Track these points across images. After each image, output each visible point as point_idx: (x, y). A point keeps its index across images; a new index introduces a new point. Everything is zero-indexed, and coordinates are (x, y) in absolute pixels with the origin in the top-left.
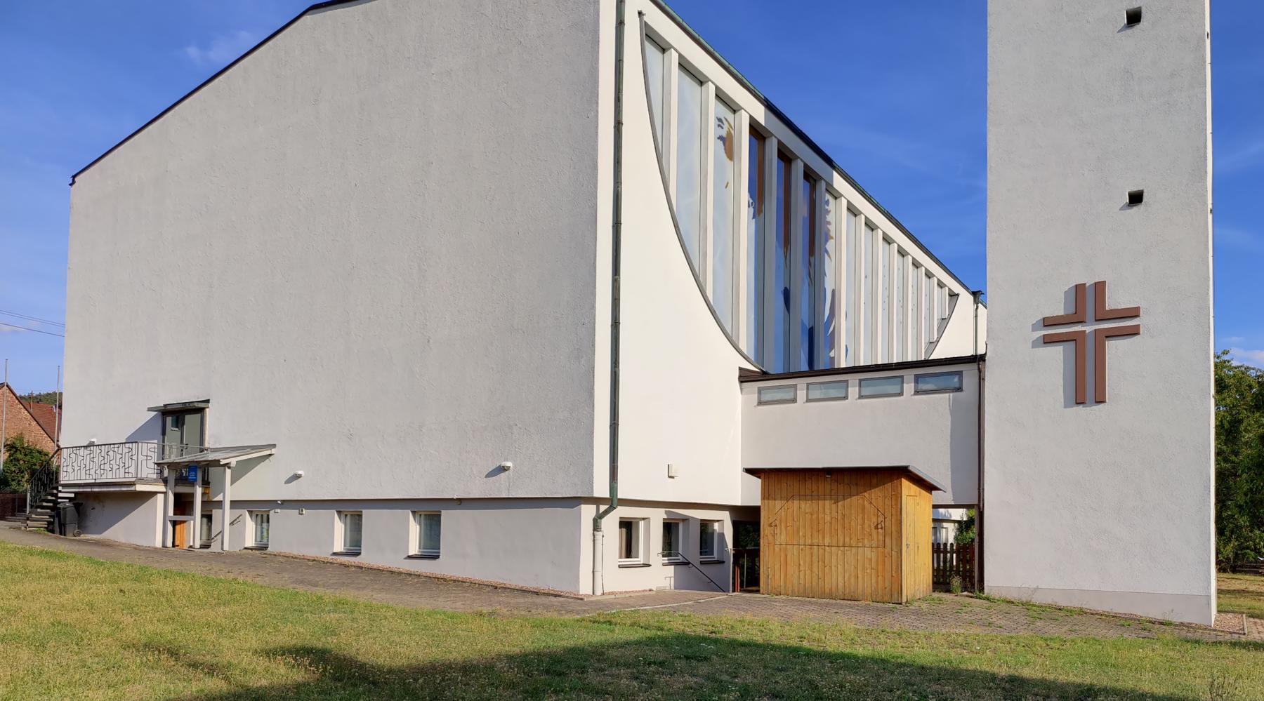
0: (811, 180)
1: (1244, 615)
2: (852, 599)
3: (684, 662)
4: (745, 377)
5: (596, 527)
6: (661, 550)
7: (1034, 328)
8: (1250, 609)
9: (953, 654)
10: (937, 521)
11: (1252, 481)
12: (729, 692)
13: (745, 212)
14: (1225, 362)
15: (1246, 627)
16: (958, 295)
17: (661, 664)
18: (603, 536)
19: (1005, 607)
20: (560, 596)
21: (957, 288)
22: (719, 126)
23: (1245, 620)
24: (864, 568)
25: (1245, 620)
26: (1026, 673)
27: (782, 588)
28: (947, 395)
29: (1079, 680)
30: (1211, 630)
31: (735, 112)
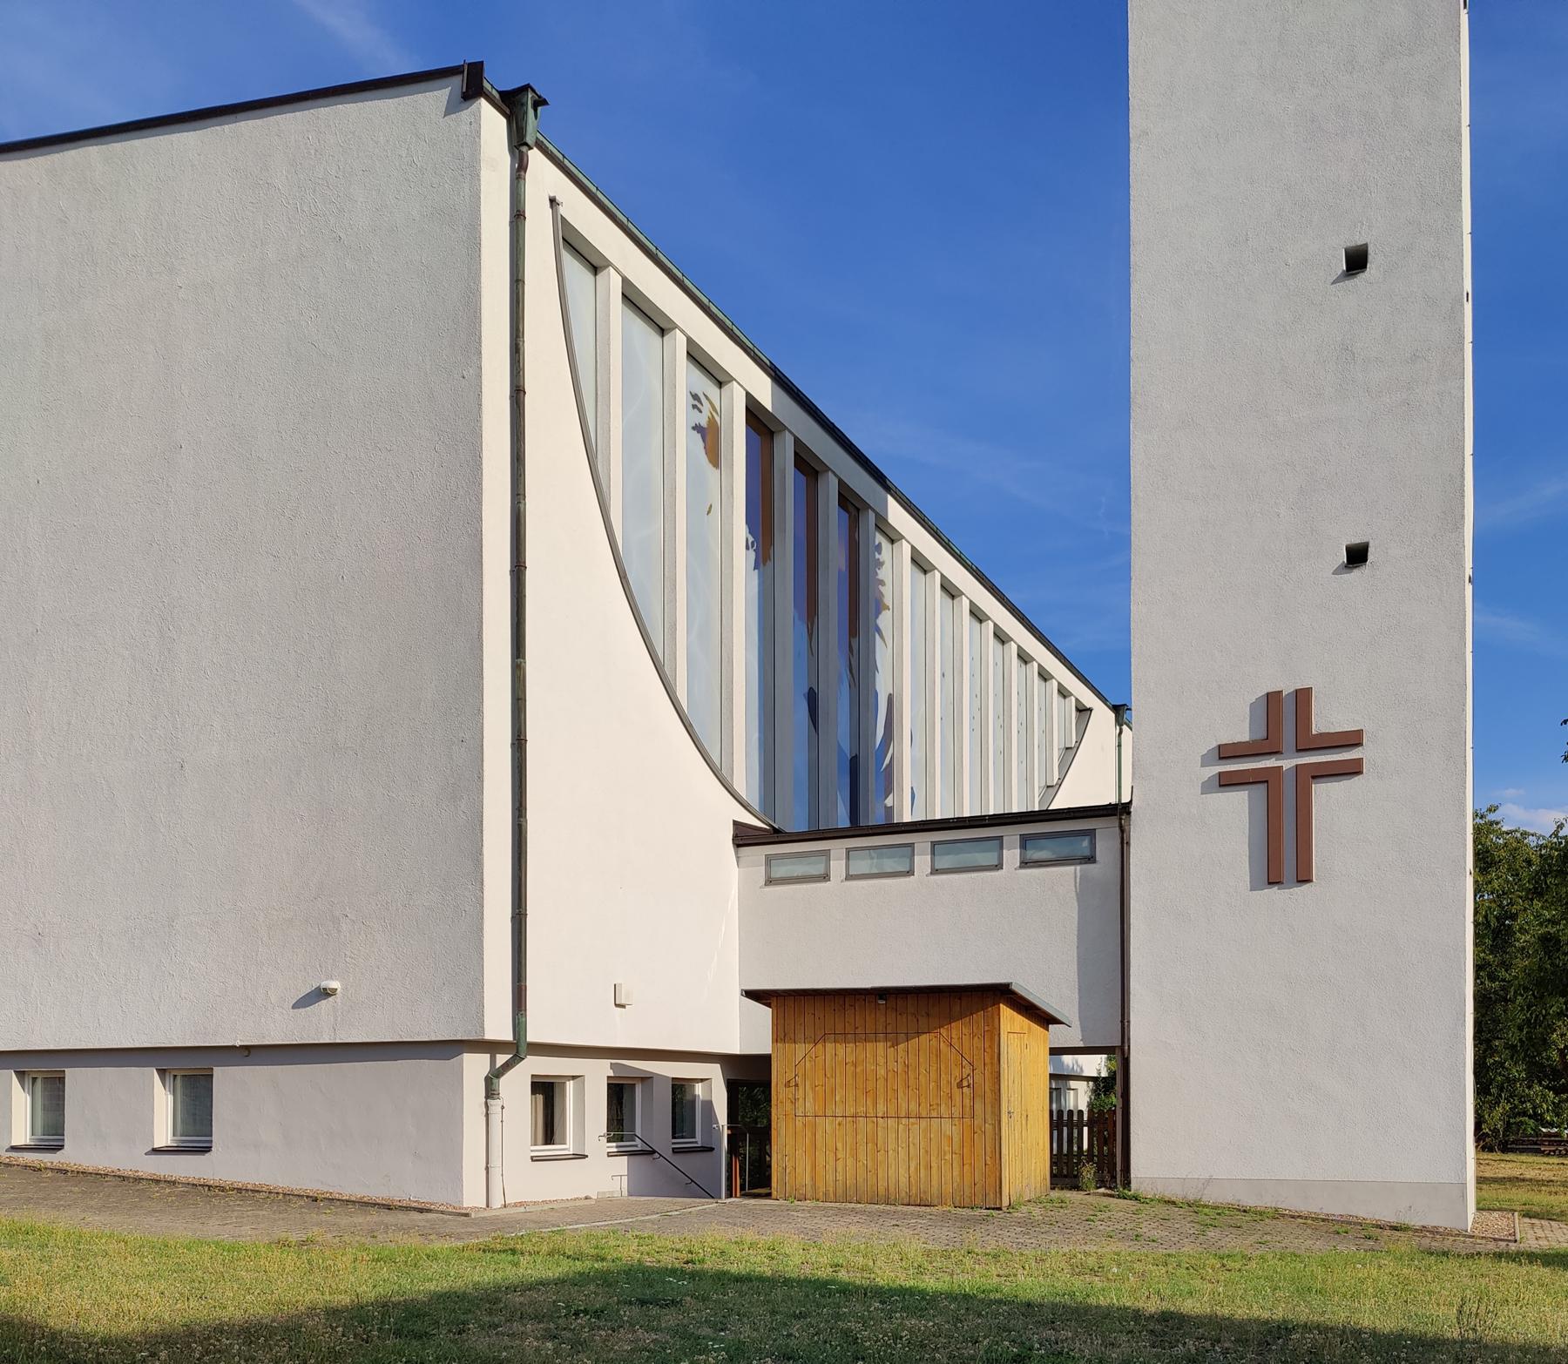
0: (851, 509)
1: (1516, 1214)
2: (923, 1203)
3: (636, 1309)
4: (744, 837)
5: (491, 1092)
6: (604, 1130)
7: (1205, 762)
8: (1525, 1204)
9: (1078, 1283)
10: (1060, 1080)
11: (1529, 1007)
12: (705, 1351)
13: (742, 558)
14: (1491, 823)
15: (1518, 1231)
16: (1090, 710)
17: (598, 1314)
18: (503, 1107)
19: (1162, 1210)
20: (429, 1211)
21: (1089, 699)
22: (694, 407)
23: (1517, 1221)
24: (941, 1154)
25: (1517, 1221)
26: (1189, 1306)
27: (809, 1188)
28: (1072, 868)
29: (1266, 1315)
30: (1465, 1236)
31: (720, 384)
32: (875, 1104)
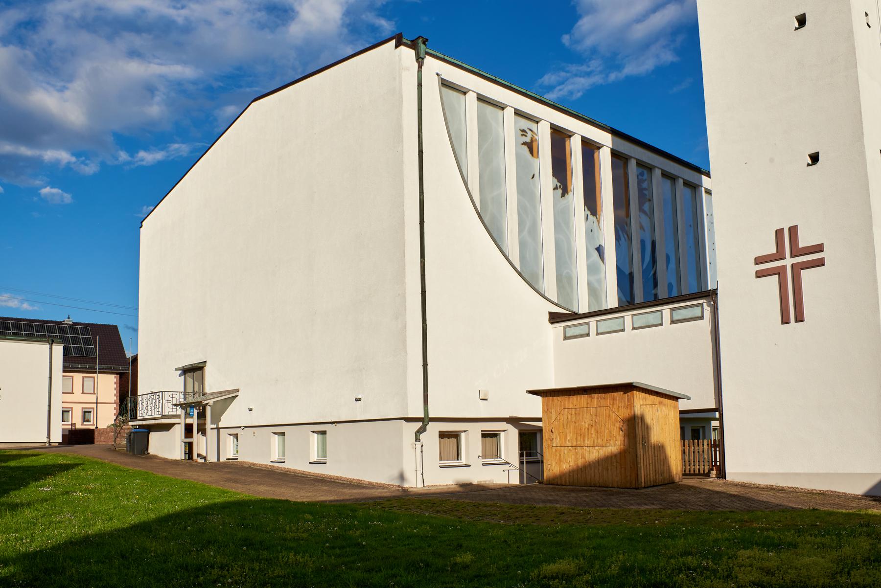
18: (422, 446)
32: (584, 440)
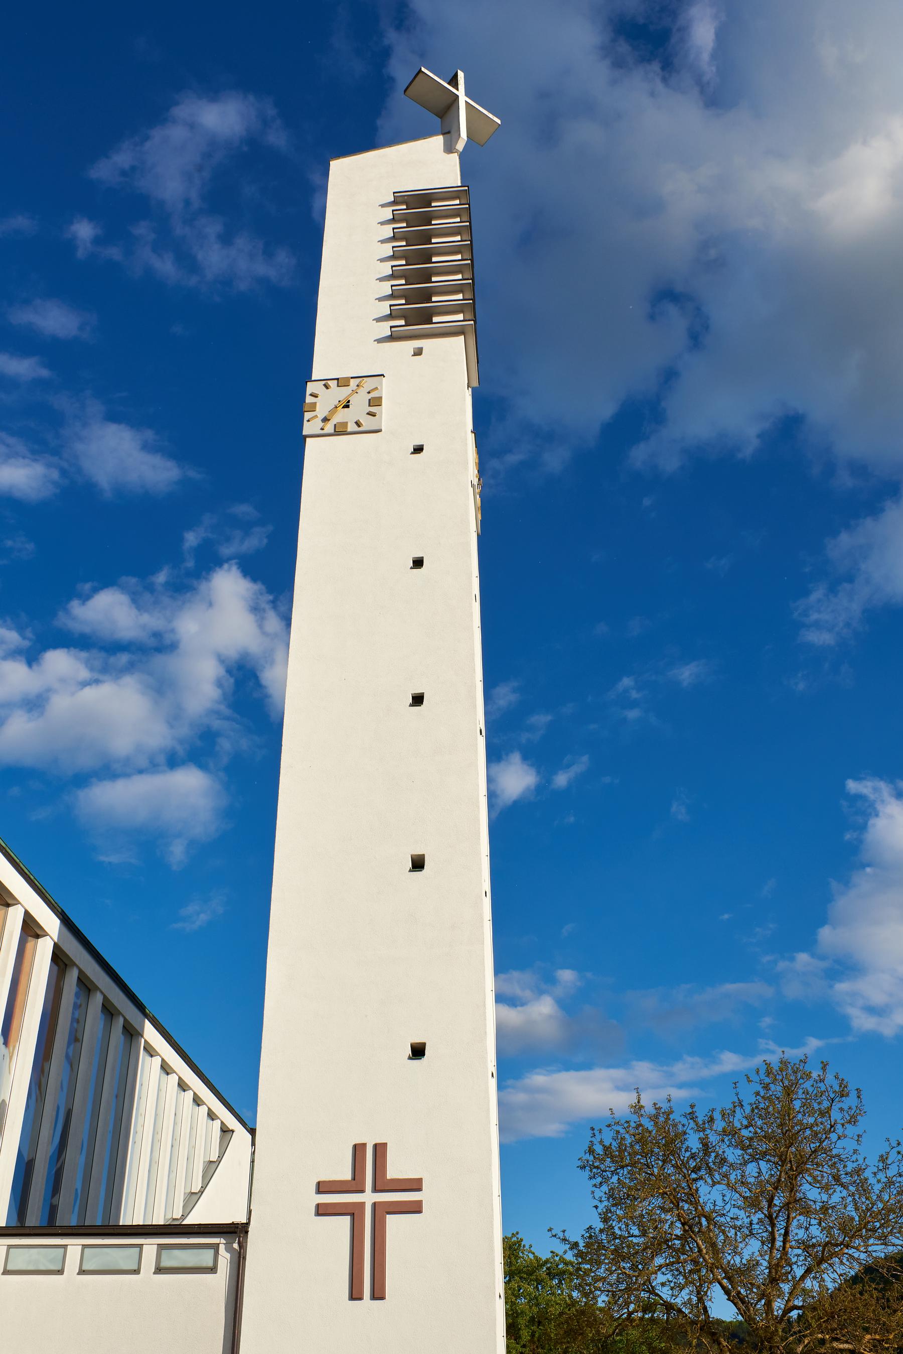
16: (233, 1131)
21: (232, 1122)
